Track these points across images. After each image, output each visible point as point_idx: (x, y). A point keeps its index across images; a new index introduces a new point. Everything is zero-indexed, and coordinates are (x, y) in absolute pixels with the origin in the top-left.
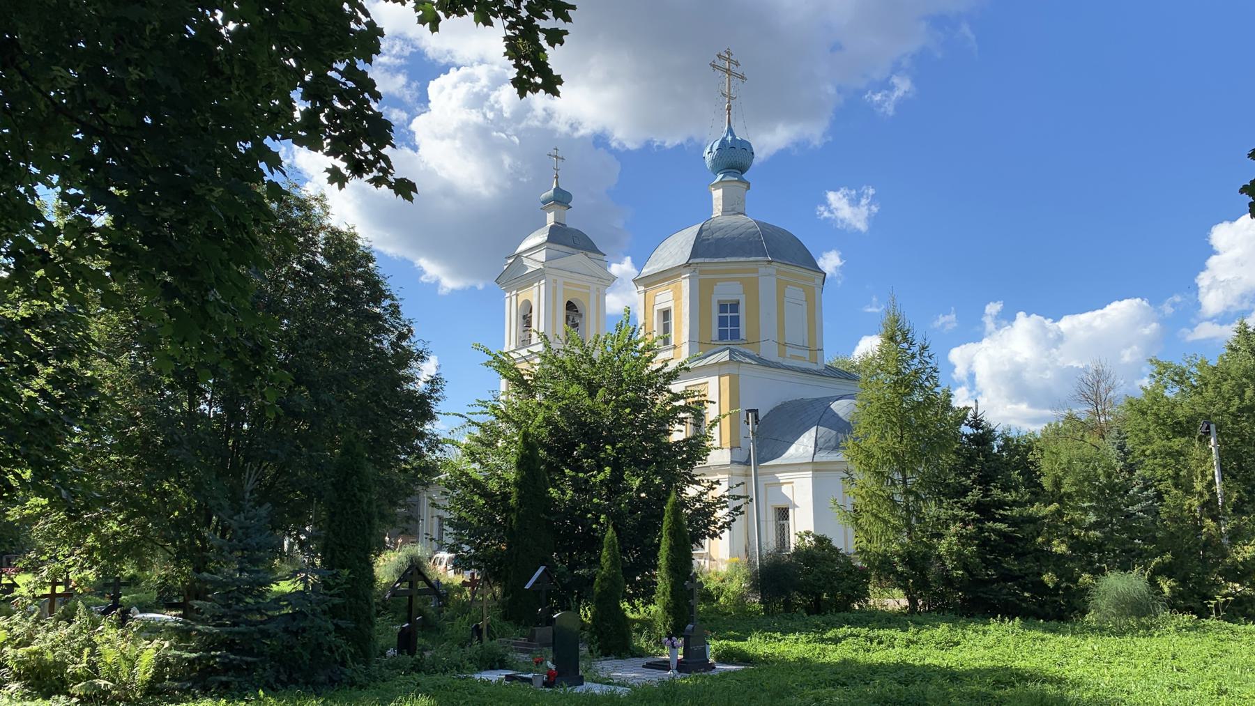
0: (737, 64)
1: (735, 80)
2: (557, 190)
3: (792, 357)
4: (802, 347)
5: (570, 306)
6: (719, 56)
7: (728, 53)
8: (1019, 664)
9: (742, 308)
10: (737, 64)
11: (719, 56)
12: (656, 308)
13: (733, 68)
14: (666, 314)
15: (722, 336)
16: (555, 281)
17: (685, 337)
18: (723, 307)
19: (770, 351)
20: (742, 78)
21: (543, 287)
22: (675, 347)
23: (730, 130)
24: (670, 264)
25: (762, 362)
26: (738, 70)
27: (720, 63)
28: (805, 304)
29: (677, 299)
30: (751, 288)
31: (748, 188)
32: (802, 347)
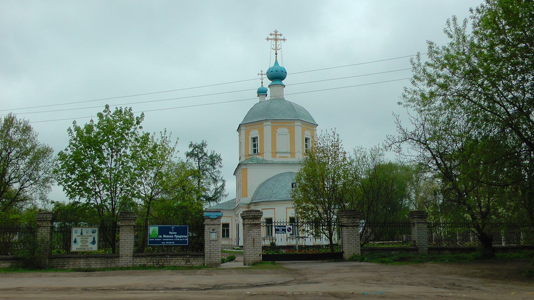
0: (281, 35)
19: (268, 156)
23: (276, 63)
26: (282, 37)
27: (270, 37)
28: (289, 134)
30: (261, 132)
32: (287, 153)
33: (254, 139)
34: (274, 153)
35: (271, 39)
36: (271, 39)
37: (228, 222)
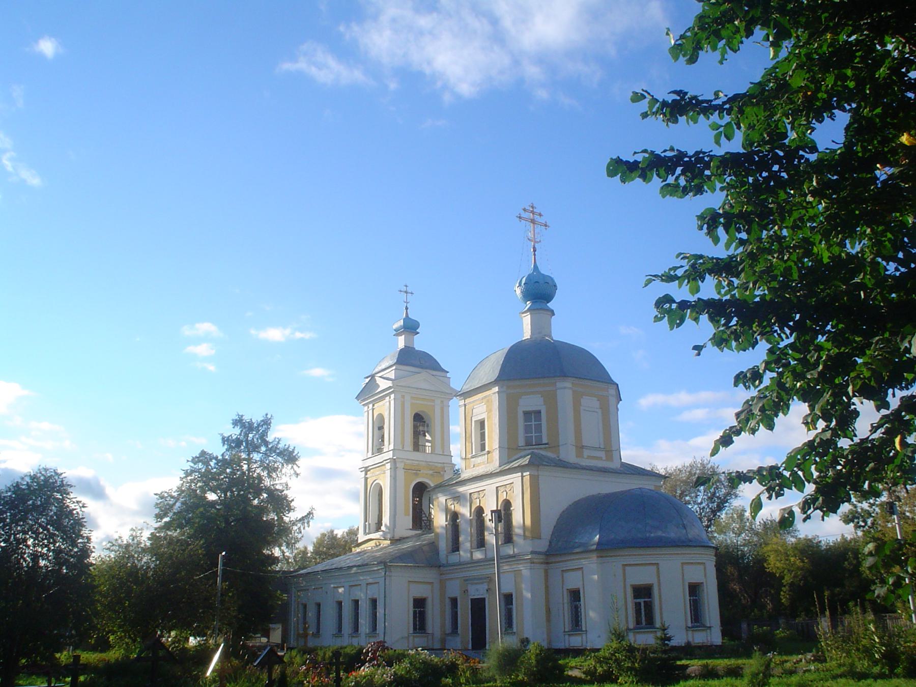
0: (540, 215)
1: (539, 228)
2: (407, 319)
3: (589, 457)
4: (598, 449)
5: (419, 420)
6: (525, 210)
7: (533, 207)
8: (702, 682)
9: (543, 415)
10: (540, 215)
11: (525, 210)
12: (474, 420)
13: (537, 217)
14: (482, 424)
15: (528, 443)
16: (403, 397)
17: (496, 445)
18: (527, 414)
19: (569, 454)
20: (546, 226)
21: (392, 402)
22: (489, 452)
23: (536, 267)
24: (485, 381)
25: (562, 465)
26: (541, 220)
27: (524, 215)
28: (600, 411)
29: (489, 411)
30: (551, 400)
31: (553, 314)
32: (598, 449)
33: (532, 416)
34: (580, 448)
35: (526, 220)
36: (526, 220)
37: (424, 596)
